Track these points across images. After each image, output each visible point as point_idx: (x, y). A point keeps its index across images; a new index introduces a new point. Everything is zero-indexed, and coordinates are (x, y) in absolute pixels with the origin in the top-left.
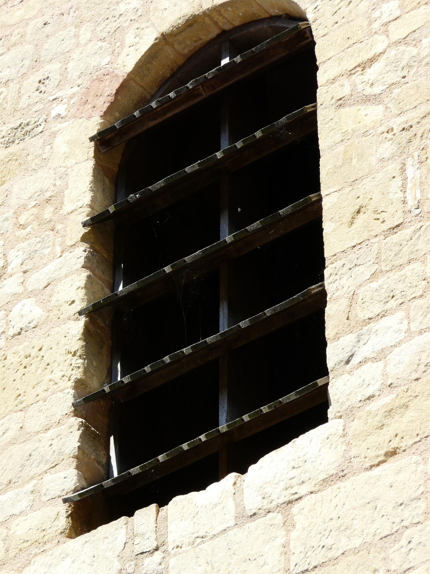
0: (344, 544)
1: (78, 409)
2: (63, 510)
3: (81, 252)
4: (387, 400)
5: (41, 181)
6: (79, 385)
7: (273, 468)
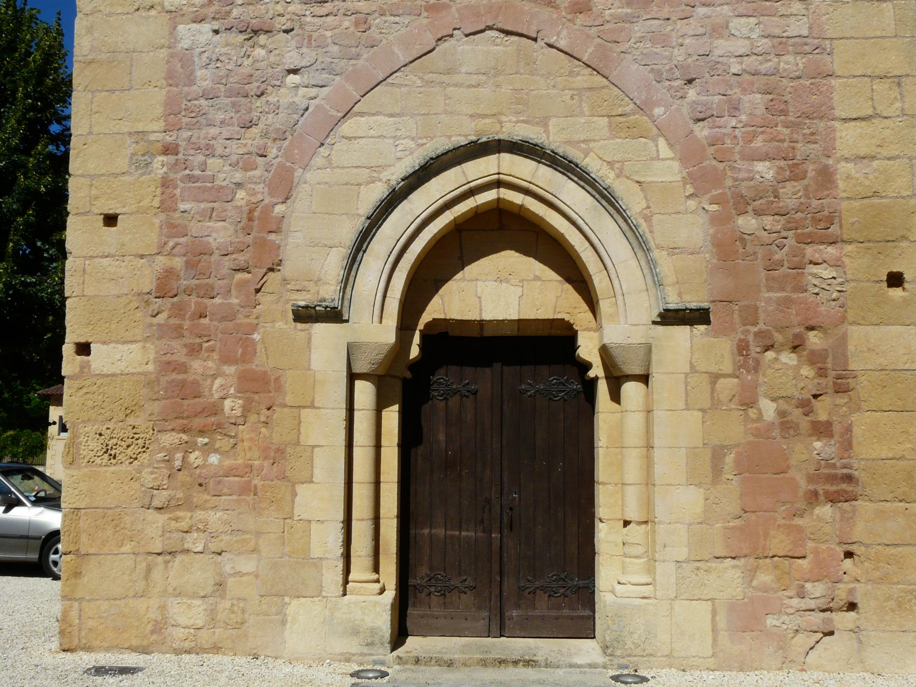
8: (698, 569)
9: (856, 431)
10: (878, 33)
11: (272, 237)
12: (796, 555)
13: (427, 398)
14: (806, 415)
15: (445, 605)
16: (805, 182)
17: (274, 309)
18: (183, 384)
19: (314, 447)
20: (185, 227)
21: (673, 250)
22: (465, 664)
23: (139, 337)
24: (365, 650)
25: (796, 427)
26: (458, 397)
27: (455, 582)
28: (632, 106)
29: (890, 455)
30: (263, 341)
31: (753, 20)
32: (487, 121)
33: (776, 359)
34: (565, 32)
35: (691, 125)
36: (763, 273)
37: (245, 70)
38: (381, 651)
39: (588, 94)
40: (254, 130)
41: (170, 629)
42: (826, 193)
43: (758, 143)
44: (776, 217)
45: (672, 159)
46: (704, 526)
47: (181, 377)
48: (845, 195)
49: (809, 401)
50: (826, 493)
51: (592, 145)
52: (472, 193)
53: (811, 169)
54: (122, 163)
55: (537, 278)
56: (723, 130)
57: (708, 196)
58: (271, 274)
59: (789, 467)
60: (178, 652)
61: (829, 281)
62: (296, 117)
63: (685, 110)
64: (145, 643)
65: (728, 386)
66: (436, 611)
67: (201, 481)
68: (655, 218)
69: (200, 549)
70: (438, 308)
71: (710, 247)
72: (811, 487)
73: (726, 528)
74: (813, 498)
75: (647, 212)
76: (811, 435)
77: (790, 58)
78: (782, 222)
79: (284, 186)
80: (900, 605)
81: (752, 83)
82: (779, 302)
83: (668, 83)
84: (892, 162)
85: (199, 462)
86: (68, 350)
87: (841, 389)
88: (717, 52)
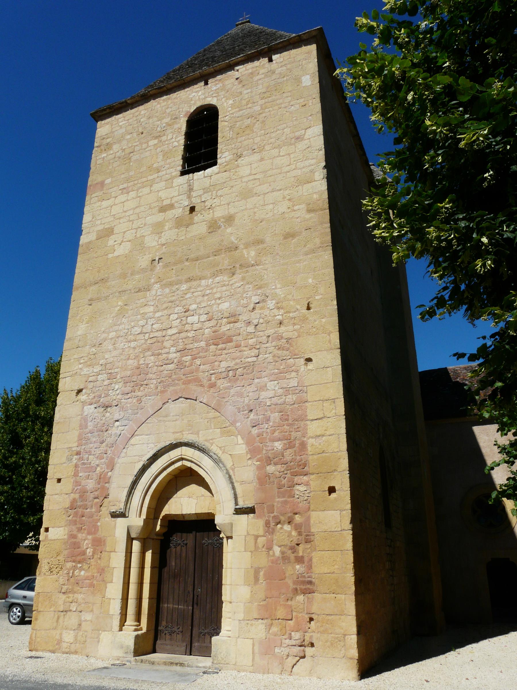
0: (218, 183)
1: (182, 159)
2: (179, 172)
3: (184, 137)
4: (225, 164)
5: (179, 126)
6: (183, 155)
7: (209, 171)
8: (248, 624)
9: (314, 560)
10: (326, 381)
11: (107, 485)
12: (287, 619)
13: (169, 547)
14: (293, 553)
15: (171, 639)
16: (294, 449)
17: (105, 512)
18: (75, 543)
19: (114, 568)
20: (81, 482)
21: (242, 482)
22: (158, 664)
23: (63, 525)
24: (125, 655)
25: (289, 558)
26: (180, 546)
27: (175, 629)
28: (229, 423)
29: (328, 571)
30: (101, 525)
31: (276, 382)
32: (179, 434)
33: (281, 528)
34: (206, 396)
35: (251, 429)
36: (277, 490)
37: (102, 422)
38: (130, 656)
39: (213, 420)
40: (104, 444)
41: (63, 643)
42: (303, 453)
43: (276, 434)
44: (283, 465)
45: (243, 444)
46: (250, 604)
47: (75, 540)
48: (311, 453)
49: (294, 547)
50: (301, 589)
51: (214, 440)
52: (173, 463)
53: (297, 443)
54: (64, 459)
55: (203, 496)
56: (262, 430)
57: (256, 458)
58: (105, 499)
59: (285, 578)
60: (64, 653)
61: (303, 492)
62: (116, 438)
63: (249, 423)
64: (54, 649)
65: (261, 541)
66: (168, 642)
67: (77, 582)
68: (236, 469)
69: (74, 610)
70: (167, 510)
71: (256, 480)
72: (295, 587)
73: (258, 605)
74: (296, 592)
75: (233, 467)
76: (295, 562)
77: (290, 396)
78: (285, 467)
79: (111, 466)
80: (332, 644)
81: (275, 409)
82: (282, 502)
83: (242, 412)
84: (331, 437)
85: (77, 574)
86: (42, 530)
87: (307, 541)
88: (261, 397)
